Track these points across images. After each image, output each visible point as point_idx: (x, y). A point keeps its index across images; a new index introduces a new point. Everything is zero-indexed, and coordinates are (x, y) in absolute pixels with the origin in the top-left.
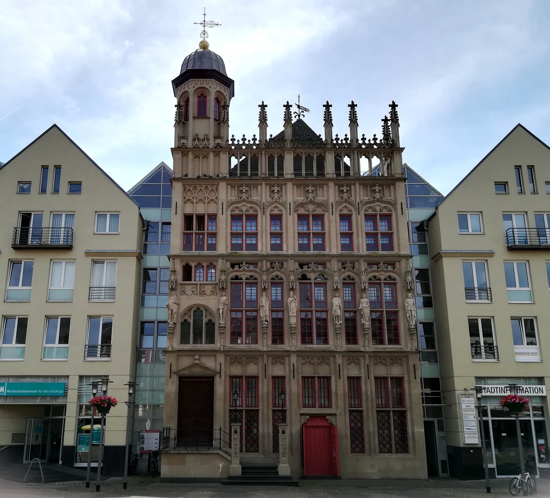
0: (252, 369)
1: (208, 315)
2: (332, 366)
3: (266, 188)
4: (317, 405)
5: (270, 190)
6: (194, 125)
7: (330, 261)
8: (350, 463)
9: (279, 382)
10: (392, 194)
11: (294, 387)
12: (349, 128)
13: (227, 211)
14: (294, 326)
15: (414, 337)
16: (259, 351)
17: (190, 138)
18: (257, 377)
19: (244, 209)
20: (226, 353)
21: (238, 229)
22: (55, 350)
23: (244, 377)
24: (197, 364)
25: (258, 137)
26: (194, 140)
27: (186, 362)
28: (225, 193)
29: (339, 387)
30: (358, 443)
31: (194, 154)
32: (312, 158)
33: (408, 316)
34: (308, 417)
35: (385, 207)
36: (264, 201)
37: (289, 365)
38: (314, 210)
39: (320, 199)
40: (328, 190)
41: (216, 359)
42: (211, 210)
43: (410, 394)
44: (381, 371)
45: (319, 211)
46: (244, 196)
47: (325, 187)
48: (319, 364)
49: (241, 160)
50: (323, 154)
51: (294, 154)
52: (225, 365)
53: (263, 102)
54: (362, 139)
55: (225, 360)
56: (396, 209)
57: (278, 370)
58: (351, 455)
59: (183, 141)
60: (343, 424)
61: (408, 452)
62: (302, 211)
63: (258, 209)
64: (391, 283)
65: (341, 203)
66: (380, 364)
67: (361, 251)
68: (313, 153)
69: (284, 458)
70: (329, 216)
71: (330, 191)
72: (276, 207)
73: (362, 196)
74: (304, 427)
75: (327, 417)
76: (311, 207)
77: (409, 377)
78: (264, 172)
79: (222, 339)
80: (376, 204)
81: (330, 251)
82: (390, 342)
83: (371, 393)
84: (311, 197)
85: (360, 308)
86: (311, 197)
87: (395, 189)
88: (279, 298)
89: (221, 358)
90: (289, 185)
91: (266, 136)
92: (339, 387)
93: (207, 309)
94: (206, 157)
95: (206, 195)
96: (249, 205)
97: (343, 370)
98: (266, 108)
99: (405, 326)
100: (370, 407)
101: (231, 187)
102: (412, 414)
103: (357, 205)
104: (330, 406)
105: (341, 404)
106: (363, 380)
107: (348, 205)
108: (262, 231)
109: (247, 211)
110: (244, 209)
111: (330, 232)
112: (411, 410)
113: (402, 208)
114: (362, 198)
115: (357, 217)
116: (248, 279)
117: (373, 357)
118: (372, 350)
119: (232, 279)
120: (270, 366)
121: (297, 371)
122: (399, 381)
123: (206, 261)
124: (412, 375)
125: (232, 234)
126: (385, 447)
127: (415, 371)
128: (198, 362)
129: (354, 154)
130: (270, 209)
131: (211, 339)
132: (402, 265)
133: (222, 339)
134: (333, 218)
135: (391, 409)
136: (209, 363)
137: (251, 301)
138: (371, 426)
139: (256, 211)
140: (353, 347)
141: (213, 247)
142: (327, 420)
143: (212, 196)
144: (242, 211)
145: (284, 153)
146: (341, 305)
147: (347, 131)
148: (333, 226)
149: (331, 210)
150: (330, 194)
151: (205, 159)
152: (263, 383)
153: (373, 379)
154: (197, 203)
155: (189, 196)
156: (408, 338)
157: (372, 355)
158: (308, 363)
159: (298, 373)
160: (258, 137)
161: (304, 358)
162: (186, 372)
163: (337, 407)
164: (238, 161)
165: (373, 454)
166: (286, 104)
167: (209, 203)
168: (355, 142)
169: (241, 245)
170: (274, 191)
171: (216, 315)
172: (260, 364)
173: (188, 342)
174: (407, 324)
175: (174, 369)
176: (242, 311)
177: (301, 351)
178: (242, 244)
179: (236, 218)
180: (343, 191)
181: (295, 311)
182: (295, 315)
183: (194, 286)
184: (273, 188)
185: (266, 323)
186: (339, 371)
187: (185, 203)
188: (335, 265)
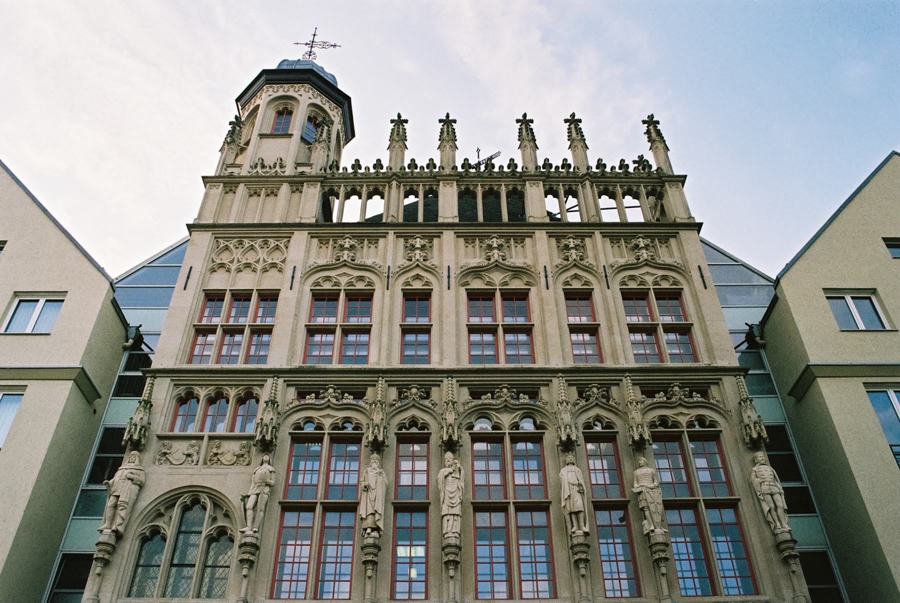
1: (220, 515)
6: (259, 147)
10: (676, 253)
13: (555, 284)
14: (453, 541)
15: (794, 567)
31: (249, 189)
32: (498, 195)
33: (766, 509)
40: (534, 245)
42: (269, 282)
45: (517, 284)
46: (496, 255)
50: (519, 188)
56: (689, 280)
62: (477, 284)
64: (707, 435)
65: (565, 269)
67: (622, 360)
70: (539, 292)
71: (538, 246)
73: (611, 256)
76: (497, 278)
78: (391, 213)
81: (548, 360)
85: (635, 490)
90: (448, 236)
91: (403, 160)
93: (218, 502)
94: (274, 193)
99: (763, 540)
107: (423, 273)
108: (381, 323)
110: (344, 280)
111: (543, 323)
113: (702, 277)
114: (612, 260)
129: (390, 187)
130: (403, 279)
134: (549, 295)
135: (318, 501)
139: (370, 284)
143: (277, 258)
146: (581, 481)
148: (548, 309)
149: (543, 280)
150: (540, 252)
151: (272, 198)
154: (239, 270)
155: (225, 258)
156: (780, 571)
167: (265, 270)
171: (238, 514)
174: (768, 533)
181: (457, 500)
182: (457, 510)
183: (193, 442)
185: (375, 534)
187: (213, 270)
188: (557, 393)
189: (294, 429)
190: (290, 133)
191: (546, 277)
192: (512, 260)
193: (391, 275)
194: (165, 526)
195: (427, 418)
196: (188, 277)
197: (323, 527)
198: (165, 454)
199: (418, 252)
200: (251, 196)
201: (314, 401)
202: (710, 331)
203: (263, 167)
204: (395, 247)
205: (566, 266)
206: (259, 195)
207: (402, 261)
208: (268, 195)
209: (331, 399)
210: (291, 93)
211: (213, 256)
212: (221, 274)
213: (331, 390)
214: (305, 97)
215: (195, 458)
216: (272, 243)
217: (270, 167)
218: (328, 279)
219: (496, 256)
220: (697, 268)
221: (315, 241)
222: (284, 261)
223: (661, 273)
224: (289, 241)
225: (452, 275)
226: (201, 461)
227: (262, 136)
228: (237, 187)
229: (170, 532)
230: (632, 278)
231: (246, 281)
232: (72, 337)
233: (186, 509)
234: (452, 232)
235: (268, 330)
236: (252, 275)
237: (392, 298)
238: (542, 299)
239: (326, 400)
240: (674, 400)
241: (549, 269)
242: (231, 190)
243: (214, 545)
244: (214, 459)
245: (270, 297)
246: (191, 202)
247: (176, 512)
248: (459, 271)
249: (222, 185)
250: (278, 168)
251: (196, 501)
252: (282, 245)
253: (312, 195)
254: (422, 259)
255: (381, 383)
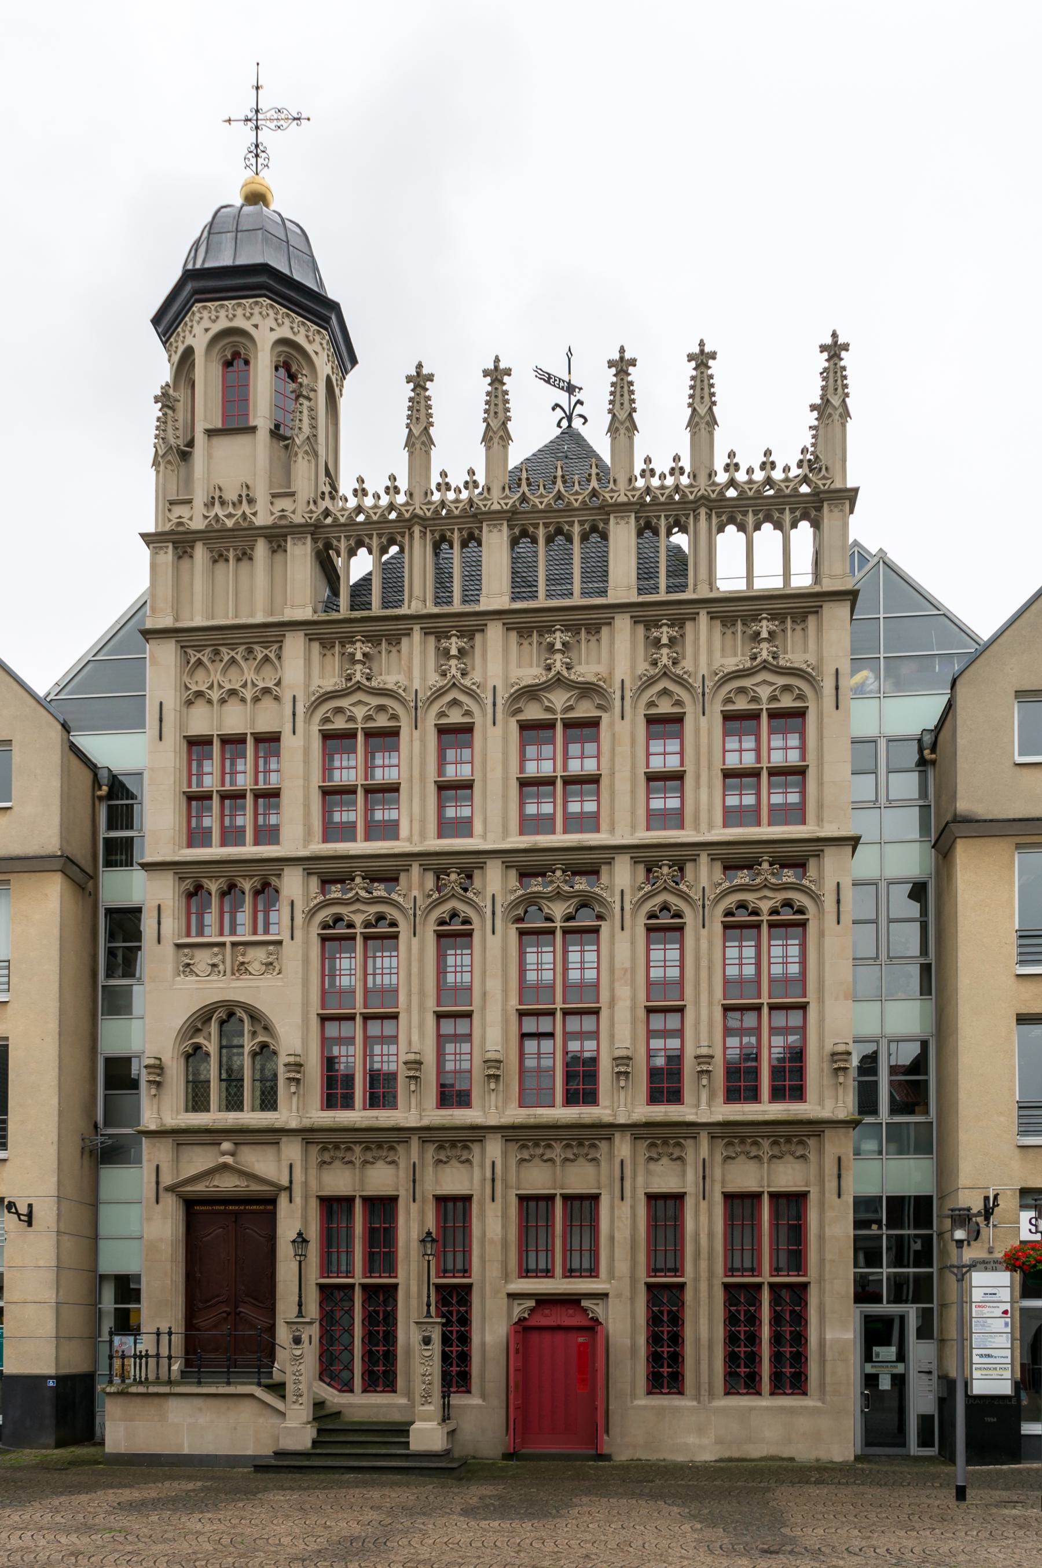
0: (381, 1179)
1: (260, 1030)
2: (604, 1164)
3: (424, 643)
4: (558, 1270)
5: (438, 649)
6: (210, 456)
7: (609, 862)
8: (654, 1426)
9: (454, 1209)
11: (493, 1228)
12: (687, 435)
13: (634, 707)
16: (810, 1122)
17: (199, 499)
18: (394, 1199)
19: (360, 712)
20: (308, 1135)
21: (542, 765)
22: (912, 1127)
23: (766, 1199)
24: (225, 1167)
25: (403, 484)
26: (210, 504)
27: (199, 1160)
28: (300, 669)
29: (622, 1225)
30: (666, 1372)
34: (532, 1303)
35: (787, 688)
36: (416, 685)
37: (482, 1166)
38: (571, 708)
39: (586, 671)
41: (279, 1151)
42: (266, 719)
43: (821, 1237)
44: (746, 1177)
45: (585, 710)
46: (764, 651)
47: (605, 630)
48: (774, 1157)
49: (385, 558)
51: (637, 519)
52: (306, 1169)
53: (702, 344)
54: (727, 468)
55: (306, 1153)
57: (453, 1180)
58: (643, 1401)
59: (179, 511)
60: (624, 1323)
61: (805, 1393)
62: (533, 712)
63: (400, 710)
66: (742, 1157)
68: (658, 518)
69: (427, 1408)
70: (612, 724)
72: (455, 702)
73: (718, 653)
74: (523, 1329)
75: (584, 1303)
76: (559, 699)
77: (822, 1192)
79: (295, 1099)
80: (758, 678)
82: (777, 1094)
83: (711, 1235)
84: (558, 664)
86: (558, 664)
87: (819, 629)
88: (794, 969)
89: (292, 1150)
90: (495, 631)
92: (622, 1225)
94: (246, 556)
95: (217, 677)
96: (376, 701)
97: (634, 1178)
98: (843, 354)
100: (704, 1275)
101: (323, 646)
102: (822, 1291)
103: (698, 684)
104: (593, 1272)
105: (622, 1267)
106: (689, 1203)
107: (462, 698)
109: (368, 718)
110: (360, 712)
112: (821, 1280)
115: (697, 721)
116: (777, 913)
117: (722, 1138)
118: (718, 1117)
119: (442, 923)
120: (430, 1170)
121: (505, 1181)
122: (792, 1205)
123: (251, 877)
124: (831, 1185)
125: (524, 783)
126: (741, 1377)
127: (839, 1176)
128: (229, 1159)
129: (696, 518)
130: (435, 708)
131: (268, 1101)
132: (833, 870)
133: (295, 1099)
134: (623, 728)
136: (266, 1165)
137: (786, 980)
138: (704, 1327)
139: (394, 717)
140: (661, 1112)
141: (268, 834)
142: (585, 1310)
144: (352, 719)
145: (480, 529)
147: (682, 443)
149: (617, 703)
151: (245, 565)
152: (408, 1212)
153: (718, 1199)
155: (200, 682)
156: (828, 1080)
157: (717, 1130)
158: (537, 1160)
159: (506, 1186)
160: (403, 484)
161: (524, 1147)
162: (200, 1187)
163: (611, 1276)
164: (377, 561)
165: (705, 1397)
166: (829, 341)
167: (256, 700)
168: (702, 481)
169: (552, 817)
170: (551, 645)
172: (402, 1164)
173: (348, 1103)
175: (167, 1180)
176: (758, 1008)
177: (311, 1130)
178: (552, 817)
179: (335, 740)
180: (659, 640)
183: (216, 950)
184: (444, 643)
186: (622, 1179)
187: (189, 703)
189: (365, 928)
190: (252, 423)
191: (623, 699)
192: (788, 656)
193: (420, 704)
194: (206, 1043)
195: (682, 905)
196: (161, 721)
197: (366, 1038)
198: (188, 965)
199: (558, 656)
200: (215, 561)
201: (339, 895)
202: (826, 779)
203: (223, 503)
204: (424, 652)
205: (652, 677)
206: (227, 560)
207: (434, 679)
208: (239, 560)
209: (360, 891)
210: (240, 323)
211: (187, 680)
212: (200, 710)
213: (559, 873)
214: (267, 325)
215: (221, 967)
216: (260, 653)
217: (234, 504)
218: (339, 710)
219: (765, 653)
220: (834, 671)
221: (513, 635)
222: (278, 684)
223: (781, 681)
224: (281, 647)
225: (500, 702)
226: (229, 972)
227: (210, 433)
228: (192, 547)
229: (212, 1047)
230: (742, 690)
231: (235, 719)
232: (37, 816)
233: (222, 1023)
234: (627, 616)
235: (274, 794)
236: (207, 707)
237: (423, 741)
238: (614, 735)
239: (354, 892)
240: (758, 881)
241: (628, 685)
242: (185, 552)
243: (191, 1059)
244: (241, 969)
245: (269, 741)
246: (122, 578)
247: (214, 1028)
248: (507, 695)
249: (170, 545)
250: (245, 506)
251: (231, 1014)
252: (272, 656)
253: (300, 557)
254: (459, 675)
255: (416, 869)
